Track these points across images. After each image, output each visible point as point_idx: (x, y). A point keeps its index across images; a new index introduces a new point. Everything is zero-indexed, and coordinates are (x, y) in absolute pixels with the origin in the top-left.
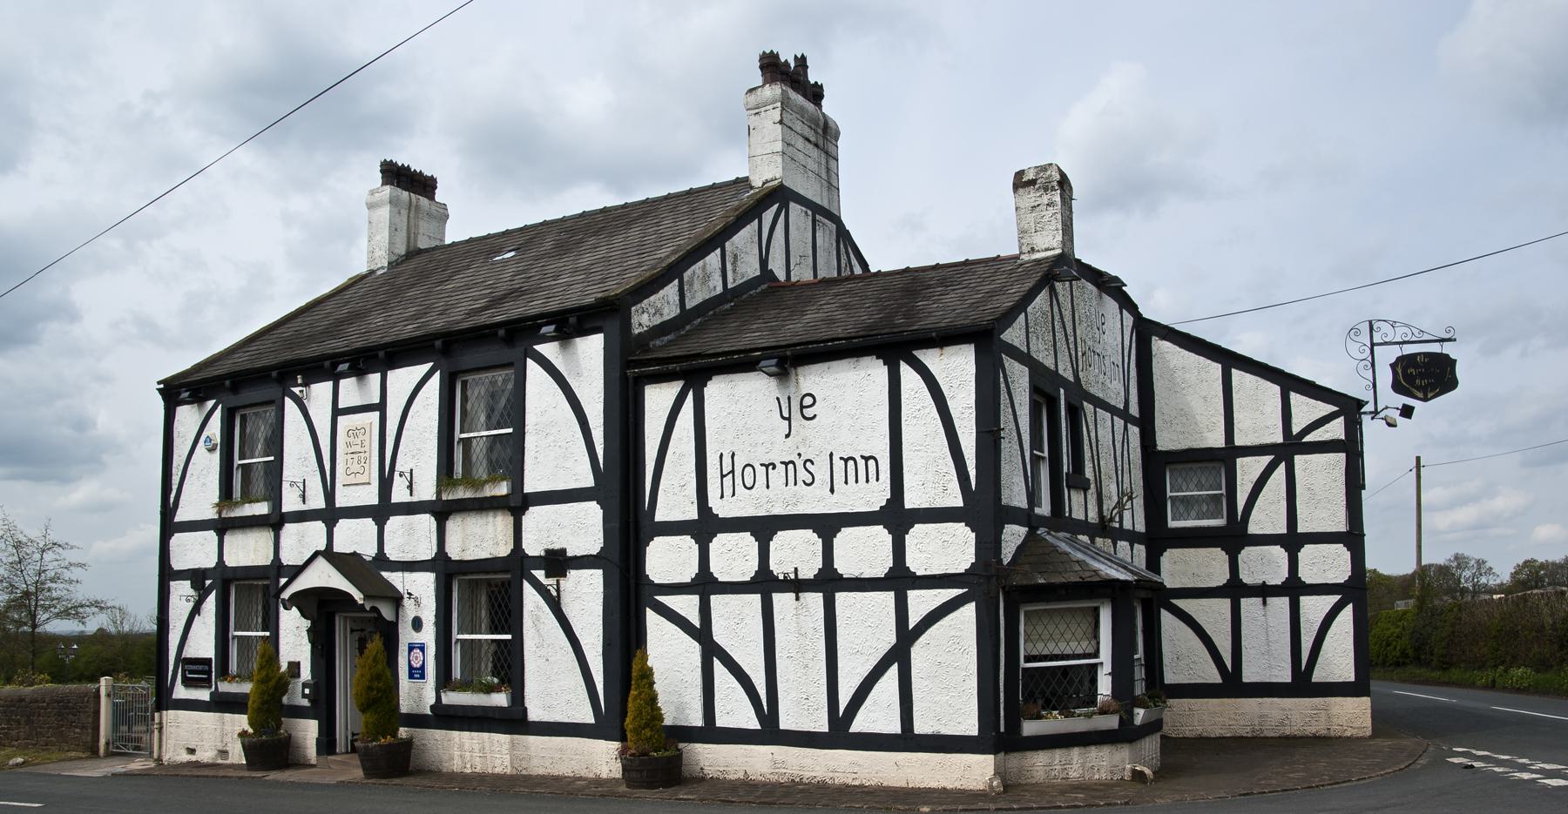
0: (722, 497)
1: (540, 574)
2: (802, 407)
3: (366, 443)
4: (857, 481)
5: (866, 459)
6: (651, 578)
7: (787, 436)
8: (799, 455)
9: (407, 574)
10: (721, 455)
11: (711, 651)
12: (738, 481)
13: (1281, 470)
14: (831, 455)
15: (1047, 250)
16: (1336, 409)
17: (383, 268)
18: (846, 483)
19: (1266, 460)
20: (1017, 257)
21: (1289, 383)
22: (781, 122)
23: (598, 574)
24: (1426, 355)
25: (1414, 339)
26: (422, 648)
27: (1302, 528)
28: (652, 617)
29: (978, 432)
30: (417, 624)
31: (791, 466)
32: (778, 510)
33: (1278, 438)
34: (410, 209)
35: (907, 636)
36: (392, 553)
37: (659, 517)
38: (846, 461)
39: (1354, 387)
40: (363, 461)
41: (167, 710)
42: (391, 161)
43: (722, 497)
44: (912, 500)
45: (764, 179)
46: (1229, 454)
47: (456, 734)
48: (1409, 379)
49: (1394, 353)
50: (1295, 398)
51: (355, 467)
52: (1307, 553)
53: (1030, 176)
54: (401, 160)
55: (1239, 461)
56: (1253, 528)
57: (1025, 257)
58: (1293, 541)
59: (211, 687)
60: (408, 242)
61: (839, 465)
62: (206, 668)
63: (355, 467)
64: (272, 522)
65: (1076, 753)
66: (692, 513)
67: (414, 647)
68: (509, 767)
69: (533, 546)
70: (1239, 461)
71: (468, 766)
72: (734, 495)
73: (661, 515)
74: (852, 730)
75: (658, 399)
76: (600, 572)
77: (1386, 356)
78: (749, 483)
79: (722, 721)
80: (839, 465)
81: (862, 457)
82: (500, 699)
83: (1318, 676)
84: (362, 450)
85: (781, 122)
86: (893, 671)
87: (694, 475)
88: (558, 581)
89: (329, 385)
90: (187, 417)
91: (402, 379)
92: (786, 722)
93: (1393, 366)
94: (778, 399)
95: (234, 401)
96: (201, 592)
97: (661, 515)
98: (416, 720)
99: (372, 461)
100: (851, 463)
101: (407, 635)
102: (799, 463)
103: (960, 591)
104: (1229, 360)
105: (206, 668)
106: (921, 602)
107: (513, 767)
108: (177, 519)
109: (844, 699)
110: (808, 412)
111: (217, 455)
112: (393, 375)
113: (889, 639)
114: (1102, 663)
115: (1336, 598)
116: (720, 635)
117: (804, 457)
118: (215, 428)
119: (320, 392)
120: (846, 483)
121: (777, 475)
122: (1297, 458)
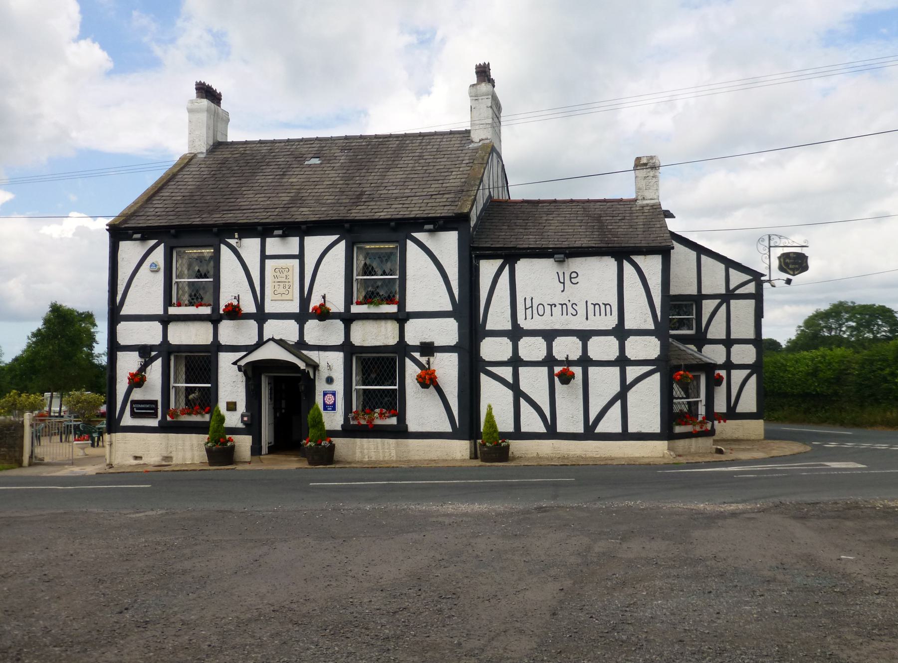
0: (526, 319)
1: (417, 355)
2: (571, 278)
3: (290, 277)
4: (600, 315)
5: (605, 305)
6: (483, 358)
7: (563, 291)
8: (569, 301)
9: (321, 353)
10: (525, 299)
11: (518, 394)
12: (535, 311)
13: (724, 307)
14: (587, 302)
15: (651, 199)
16: (751, 278)
17: (202, 153)
18: (595, 315)
19: (717, 301)
20: (635, 200)
21: (729, 264)
22: (491, 107)
23: (454, 357)
24: (795, 253)
25: (789, 245)
26: (334, 394)
27: (733, 336)
28: (483, 378)
29: (662, 296)
30: (330, 380)
31: (564, 306)
32: (557, 327)
33: (723, 291)
34: (214, 116)
35: (625, 388)
36: (309, 339)
37: (488, 327)
38: (595, 305)
39: (761, 268)
40: (287, 287)
41: (115, 433)
42: (200, 82)
43: (526, 319)
44: (628, 325)
45: (480, 138)
46: (699, 298)
47: (358, 440)
48: (787, 264)
49: (779, 252)
50: (731, 271)
51: (281, 290)
52: (735, 349)
53: (644, 161)
54: (208, 82)
55: (704, 302)
56: (710, 336)
57: (639, 202)
58: (728, 343)
59: (157, 417)
60: (214, 137)
61: (591, 307)
62: (154, 406)
63: (281, 290)
64: (213, 319)
65: (694, 440)
66: (508, 326)
67: (328, 393)
68: (395, 457)
69: (412, 339)
70: (704, 302)
71: (367, 457)
72: (532, 318)
73: (489, 326)
74: (596, 431)
75: (488, 268)
76: (456, 354)
77: (778, 252)
78: (541, 312)
79: (524, 429)
80: (591, 307)
81: (603, 304)
82: (393, 421)
83: (740, 409)
84: (287, 281)
85: (491, 107)
86: (618, 404)
87: (509, 307)
88: (429, 359)
89: (257, 241)
90: (130, 251)
91: (315, 244)
92: (560, 428)
93: (779, 258)
94: (558, 273)
95: (174, 242)
96: (147, 359)
97: (489, 326)
98: (334, 434)
99: (294, 287)
100: (597, 306)
101: (321, 387)
102: (569, 305)
103: (653, 367)
104: (700, 250)
105: (154, 406)
106: (633, 372)
107: (397, 456)
108: (122, 313)
109: (592, 417)
110: (574, 281)
111: (161, 276)
112: (308, 240)
113: (617, 388)
114: (701, 401)
115: (748, 371)
116: (524, 386)
117: (572, 302)
118: (159, 255)
119: (250, 247)
120: (595, 315)
121: (557, 310)
122: (732, 301)
